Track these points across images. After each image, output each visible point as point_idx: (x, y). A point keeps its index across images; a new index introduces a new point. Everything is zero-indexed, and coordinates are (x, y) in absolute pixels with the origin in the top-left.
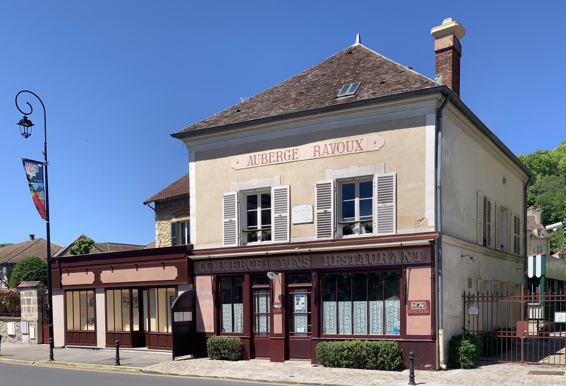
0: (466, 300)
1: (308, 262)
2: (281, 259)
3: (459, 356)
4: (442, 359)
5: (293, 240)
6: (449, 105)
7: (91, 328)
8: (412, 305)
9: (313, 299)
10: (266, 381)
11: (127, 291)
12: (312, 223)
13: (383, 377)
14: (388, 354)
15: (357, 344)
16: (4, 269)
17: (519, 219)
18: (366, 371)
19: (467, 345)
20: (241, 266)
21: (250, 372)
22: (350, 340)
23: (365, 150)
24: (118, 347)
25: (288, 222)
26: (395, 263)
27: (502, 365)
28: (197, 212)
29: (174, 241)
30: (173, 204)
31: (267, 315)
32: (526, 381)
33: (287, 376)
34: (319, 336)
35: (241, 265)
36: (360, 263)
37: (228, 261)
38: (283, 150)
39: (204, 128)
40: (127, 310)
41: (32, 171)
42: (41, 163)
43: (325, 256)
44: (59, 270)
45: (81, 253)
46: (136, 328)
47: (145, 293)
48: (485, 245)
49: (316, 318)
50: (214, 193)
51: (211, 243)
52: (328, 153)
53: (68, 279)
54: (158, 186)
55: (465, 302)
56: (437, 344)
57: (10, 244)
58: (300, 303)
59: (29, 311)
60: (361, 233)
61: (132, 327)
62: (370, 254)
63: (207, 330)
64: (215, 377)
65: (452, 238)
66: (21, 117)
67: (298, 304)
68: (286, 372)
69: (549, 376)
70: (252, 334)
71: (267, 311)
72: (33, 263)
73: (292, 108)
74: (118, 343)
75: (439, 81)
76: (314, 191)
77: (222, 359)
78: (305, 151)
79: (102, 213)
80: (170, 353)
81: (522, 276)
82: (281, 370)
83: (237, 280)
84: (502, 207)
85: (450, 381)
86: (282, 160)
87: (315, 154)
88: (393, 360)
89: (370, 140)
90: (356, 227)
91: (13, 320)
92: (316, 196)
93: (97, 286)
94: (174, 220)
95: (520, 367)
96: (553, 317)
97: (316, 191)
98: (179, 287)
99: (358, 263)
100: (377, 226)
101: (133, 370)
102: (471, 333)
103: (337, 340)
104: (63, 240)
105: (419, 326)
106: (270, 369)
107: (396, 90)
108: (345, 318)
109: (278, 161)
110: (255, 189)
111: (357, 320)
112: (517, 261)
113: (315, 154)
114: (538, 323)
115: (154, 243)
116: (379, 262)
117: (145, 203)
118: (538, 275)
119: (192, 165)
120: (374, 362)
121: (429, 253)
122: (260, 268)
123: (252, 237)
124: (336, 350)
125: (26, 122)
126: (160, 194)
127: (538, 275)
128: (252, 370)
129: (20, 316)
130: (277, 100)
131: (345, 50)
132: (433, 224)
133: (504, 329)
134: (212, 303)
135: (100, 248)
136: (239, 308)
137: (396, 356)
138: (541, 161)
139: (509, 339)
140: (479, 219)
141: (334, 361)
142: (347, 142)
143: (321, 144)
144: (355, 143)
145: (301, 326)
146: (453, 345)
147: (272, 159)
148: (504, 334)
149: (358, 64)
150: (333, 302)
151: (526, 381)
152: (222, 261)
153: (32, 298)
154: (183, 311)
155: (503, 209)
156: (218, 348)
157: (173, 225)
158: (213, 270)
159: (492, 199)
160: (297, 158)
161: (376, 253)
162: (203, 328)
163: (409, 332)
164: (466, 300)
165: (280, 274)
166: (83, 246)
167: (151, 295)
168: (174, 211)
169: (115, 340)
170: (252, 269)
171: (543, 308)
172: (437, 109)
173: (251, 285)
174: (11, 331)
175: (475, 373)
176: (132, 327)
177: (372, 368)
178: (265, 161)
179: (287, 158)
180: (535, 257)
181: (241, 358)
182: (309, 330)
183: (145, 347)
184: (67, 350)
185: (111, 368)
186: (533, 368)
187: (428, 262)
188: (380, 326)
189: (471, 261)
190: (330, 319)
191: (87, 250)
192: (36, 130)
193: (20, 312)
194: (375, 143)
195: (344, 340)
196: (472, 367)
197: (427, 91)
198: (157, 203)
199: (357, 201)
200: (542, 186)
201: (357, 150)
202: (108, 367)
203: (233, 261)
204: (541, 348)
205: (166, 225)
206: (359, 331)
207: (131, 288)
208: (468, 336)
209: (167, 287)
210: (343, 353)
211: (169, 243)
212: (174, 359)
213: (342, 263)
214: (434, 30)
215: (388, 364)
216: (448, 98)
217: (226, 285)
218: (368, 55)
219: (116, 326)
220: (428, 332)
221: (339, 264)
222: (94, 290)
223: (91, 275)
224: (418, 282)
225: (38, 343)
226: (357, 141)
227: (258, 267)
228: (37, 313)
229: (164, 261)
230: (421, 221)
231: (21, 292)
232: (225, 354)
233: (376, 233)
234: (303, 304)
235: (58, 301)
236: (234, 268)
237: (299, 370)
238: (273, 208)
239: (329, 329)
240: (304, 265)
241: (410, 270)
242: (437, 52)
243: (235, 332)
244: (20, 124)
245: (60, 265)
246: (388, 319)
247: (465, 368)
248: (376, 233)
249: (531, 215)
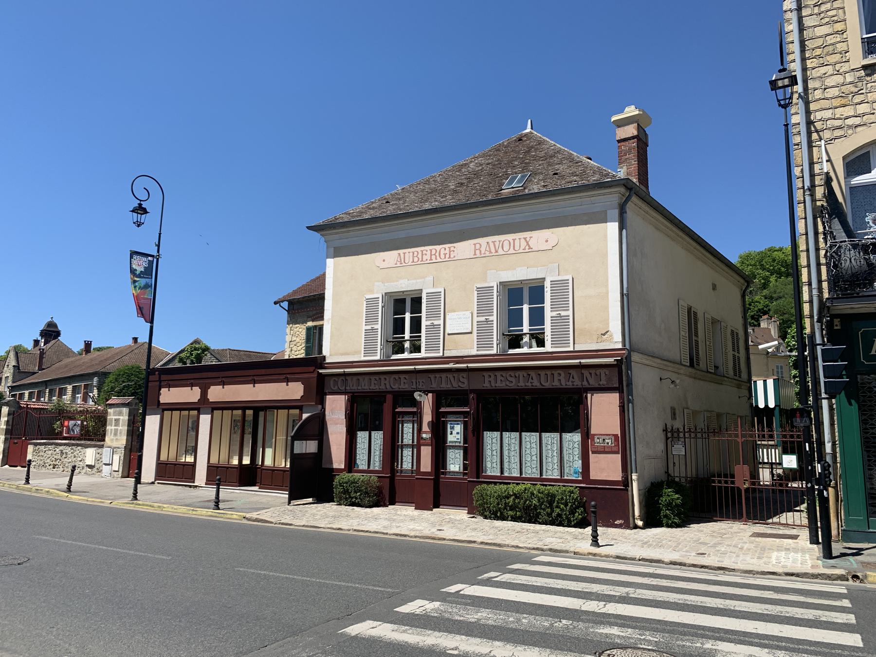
0: (669, 435)
1: (465, 381)
2: (432, 376)
3: (660, 510)
4: (637, 513)
5: (448, 354)
6: (634, 198)
7: (190, 459)
8: (597, 440)
9: (470, 428)
10: (405, 536)
11: (240, 412)
12: (471, 333)
13: (559, 535)
14: (566, 505)
15: (525, 489)
16: (96, 379)
17: (737, 334)
18: (538, 527)
19: (670, 495)
20: (382, 384)
21: (386, 523)
22: (518, 484)
23: (534, 249)
24: (218, 485)
25: (442, 332)
27: (719, 523)
29: (308, 350)
30: (306, 306)
31: (413, 446)
32: (746, 546)
33: (434, 530)
34: (478, 477)
35: (383, 382)
36: (529, 384)
37: (367, 378)
38: (438, 247)
39: (346, 220)
40: (237, 438)
41: (140, 265)
42: (152, 256)
43: (486, 374)
44: (158, 383)
45: (192, 362)
46: (246, 461)
47: (262, 414)
48: (692, 365)
50: (354, 293)
51: (347, 354)
52: (490, 252)
53: (168, 395)
54: (292, 284)
55: (667, 439)
56: (630, 493)
57: (109, 348)
58: (454, 432)
59: (115, 434)
60: (531, 347)
61: (240, 460)
62: (542, 373)
63: (335, 466)
64: (339, 529)
65: (646, 357)
66: (136, 203)
67: (451, 433)
68: (433, 524)
69: (778, 540)
70: (393, 471)
72: (129, 373)
73: (449, 201)
74: (219, 480)
75: (622, 173)
77: (353, 504)
78: (464, 248)
79: (219, 312)
80: (285, 496)
81: (748, 405)
82: (427, 520)
83: (377, 401)
84: (713, 318)
85: (646, 543)
88: (573, 512)
89: (540, 238)
90: (524, 340)
91: (95, 446)
92: (476, 301)
93: (203, 405)
95: (743, 526)
96: (799, 461)
97: (476, 295)
98: (304, 409)
100: (550, 340)
101: (235, 516)
102: (677, 479)
103: (501, 483)
104: (170, 342)
105: (606, 468)
106: (413, 519)
107: (571, 182)
108: (512, 454)
110: (403, 292)
111: (527, 458)
112: (739, 387)
114: (772, 469)
115: (283, 352)
117: (275, 303)
118: (772, 405)
119: (330, 262)
120: (549, 515)
121: (616, 374)
122: (407, 386)
123: (399, 348)
124: (499, 496)
125: (140, 210)
126: (295, 292)
127: (772, 405)
128: (389, 520)
129: (104, 440)
130: (433, 191)
131: (514, 137)
132: (620, 339)
133: (719, 476)
134: (344, 430)
135: (217, 356)
136: (378, 437)
137: (578, 507)
138: (774, 260)
139: (720, 487)
140: (683, 333)
141: (497, 512)
142: (514, 240)
143: (483, 241)
144: (523, 241)
145: (455, 463)
146: (651, 495)
147: (425, 258)
148: (720, 482)
149: (528, 152)
151: (746, 546)
152: (359, 377)
153: (121, 418)
154: (306, 440)
155: (714, 322)
156: (348, 490)
157: (309, 329)
159: (700, 308)
161: (549, 372)
162: (331, 462)
163: (594, 475)
164: (669, 435)
165: (430, 395)
166: (195, 353)
167: (268, 418)
168: (311, 313)
169: (219, 475)
170: (396, 387)
171: (780, 448)
172: (619, 204)
173: (394, 408)
174: (90, 461)
175: (681, 534)
176: (240, 460)
177: (545, 523)
178: (416, 259)
179: (442, 256)
180: (765, 381)
181: (377, 504)
182: (465, 467)
183: (255, 485)
184: (157, 487)
185: (206, 513)
186: (760, 528)
188: (555, 467)
189: (672, 386)
190: (492, 455)
191: (199, 358)
192: (151, 220)
193: (104, 435)
194: (547, 241)
195: (509, 483)
196: (678, 526)
197: (607, 185)
198: (291, 303)
199: (526, 308)
200: (778, 291)
202: (204, 512)
203: (373, 378)
204: (775, 503)
207: (244, 409)
208: (671, 482)
209: (289, 408)
210: (507, 501)
211: (303, 351)
212: (289, 503)
213: (508, 383)
214: (614, 118)
215: (567, 518)
216: (633, 192)
217: (366, 407)
218: (541, 143)
219: (220, 457)
220: (617, 475)
222: (198, 410)
223: (197, 391)
224: (604, 411)
225: (122, 477)
226: (525, 239)
227: (404, 385)
228: (125, 438)
229: (288, 376)
230: (604, 335)
231: (109, 410)
232: (356, 498)
233: (548, 347)
234: (458, 433)
235: (152, 423)
236: (374, 386)
237: (451, 521)
238: (424, 314)
239: (491, 468)
240: (460, 384)
241: (592, 395)
242: (619, 141)
243: (371, 468)
244: (132, 211)
245: (160, 378)
246: (566, 458)
247: (668, 526)
248: (548, 347)
249: (766, 326)
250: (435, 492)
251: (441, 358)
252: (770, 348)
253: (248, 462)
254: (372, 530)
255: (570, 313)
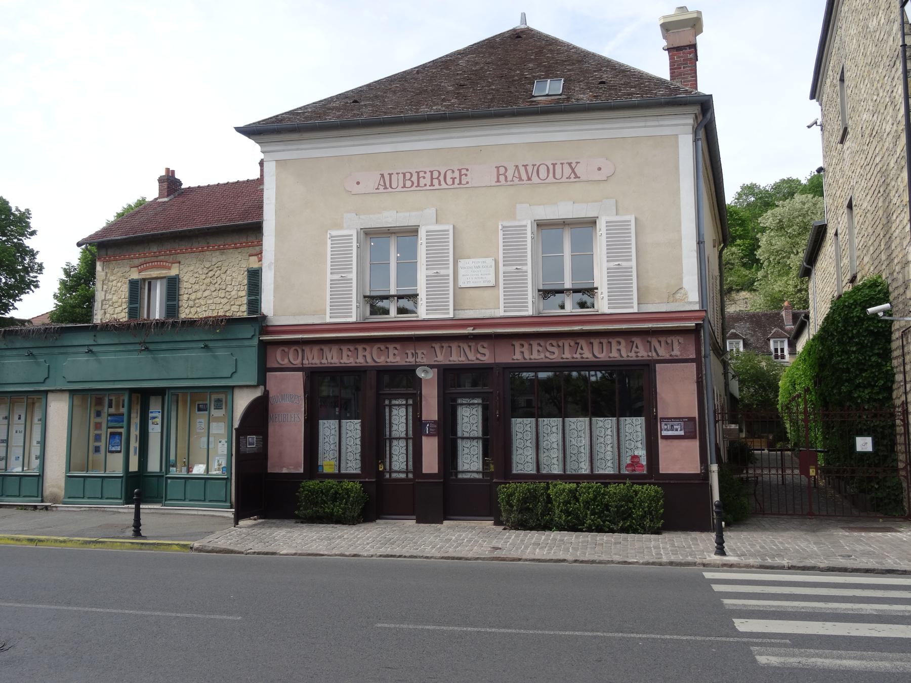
26: (637, 356)
28: (276, 260)
36: (578, 356)
49: (497, 444)
52: (521, 179)
64: (355, 555)
71: (407, 434)
76: (326, 243)
80: (230, 513)
86: (440, 184)
87: (498, 178)
94: (135, 275)
99: (575, 356)
105: (680, 458)
108: (553, 446)
109: (432, 185)
113: (498, 178)
116: (611, 355)
136: (353, 428)
142: (554, 165)
144: (566, 167)
145: (471, 460)
150: (332, 421)
158: (305, 362)
160: (467, 183)
178: (408, 184)
179: (449, 181)
187: (691, 357)
201: (569, 178)
205: (119, 284)
206: (603, 466)
211: (123, 314)
213: (548, 354)
221: (542, 356)
226: (570, 164)
239: (523, 460)
240: (479, 356)
250: (441, 499)
251: (452, 319)
252: (880, 311)
253: (859, 448)
254: (407, 555)
255: (634, 263)
